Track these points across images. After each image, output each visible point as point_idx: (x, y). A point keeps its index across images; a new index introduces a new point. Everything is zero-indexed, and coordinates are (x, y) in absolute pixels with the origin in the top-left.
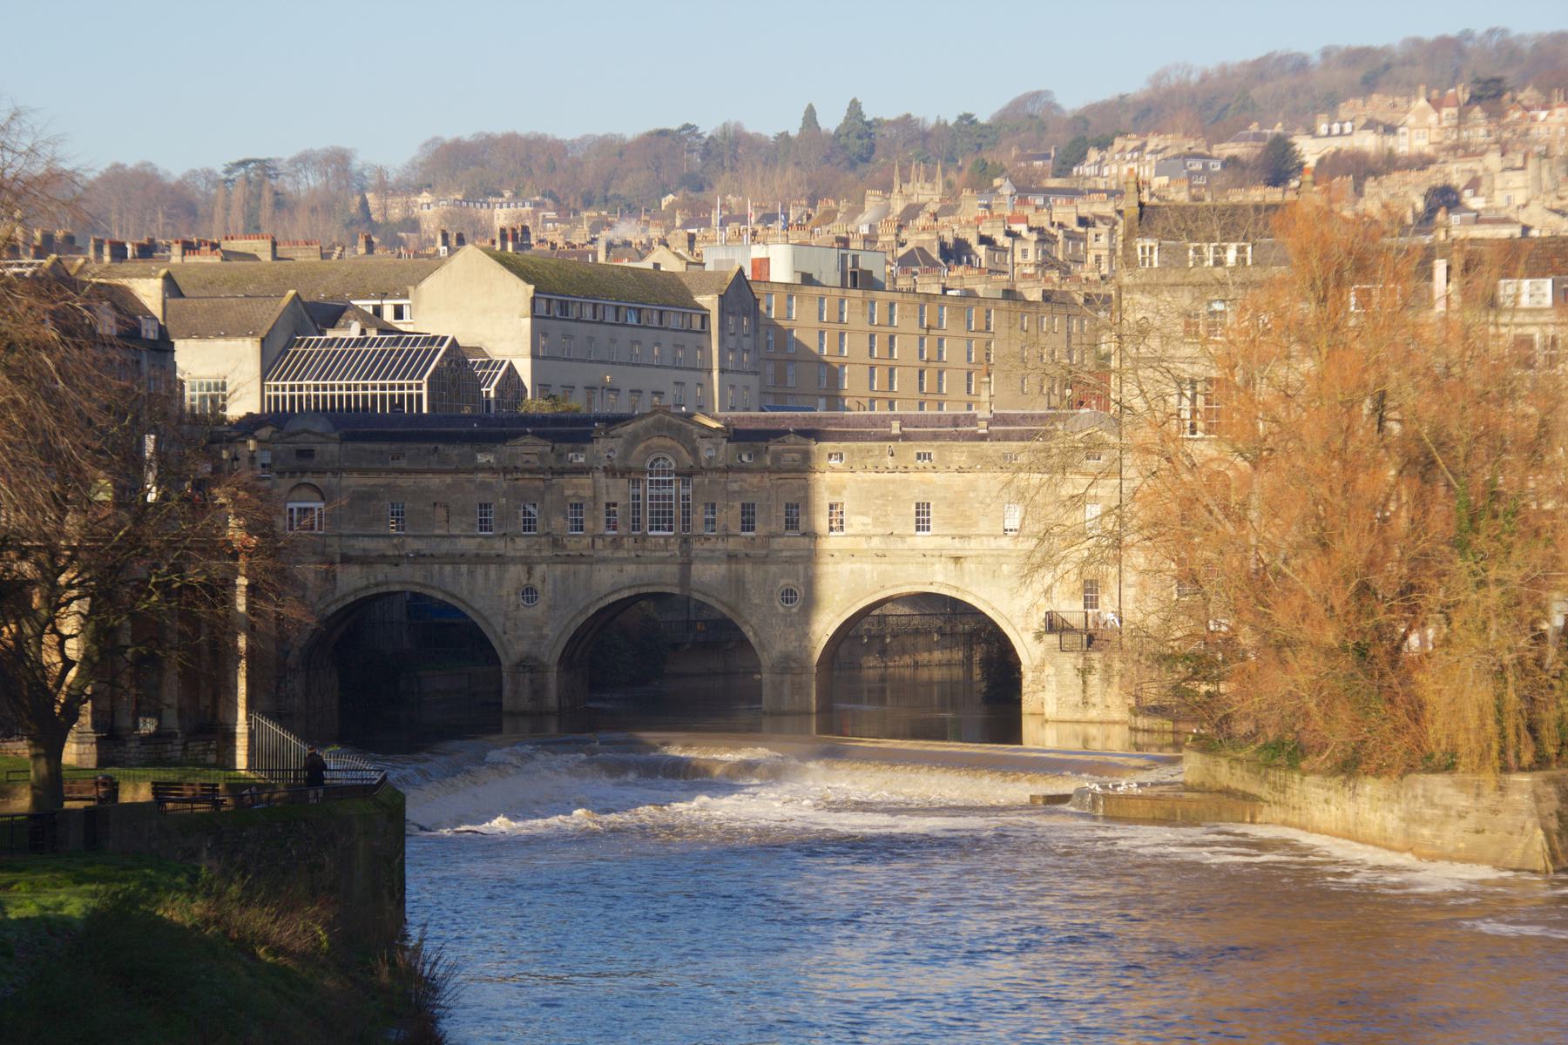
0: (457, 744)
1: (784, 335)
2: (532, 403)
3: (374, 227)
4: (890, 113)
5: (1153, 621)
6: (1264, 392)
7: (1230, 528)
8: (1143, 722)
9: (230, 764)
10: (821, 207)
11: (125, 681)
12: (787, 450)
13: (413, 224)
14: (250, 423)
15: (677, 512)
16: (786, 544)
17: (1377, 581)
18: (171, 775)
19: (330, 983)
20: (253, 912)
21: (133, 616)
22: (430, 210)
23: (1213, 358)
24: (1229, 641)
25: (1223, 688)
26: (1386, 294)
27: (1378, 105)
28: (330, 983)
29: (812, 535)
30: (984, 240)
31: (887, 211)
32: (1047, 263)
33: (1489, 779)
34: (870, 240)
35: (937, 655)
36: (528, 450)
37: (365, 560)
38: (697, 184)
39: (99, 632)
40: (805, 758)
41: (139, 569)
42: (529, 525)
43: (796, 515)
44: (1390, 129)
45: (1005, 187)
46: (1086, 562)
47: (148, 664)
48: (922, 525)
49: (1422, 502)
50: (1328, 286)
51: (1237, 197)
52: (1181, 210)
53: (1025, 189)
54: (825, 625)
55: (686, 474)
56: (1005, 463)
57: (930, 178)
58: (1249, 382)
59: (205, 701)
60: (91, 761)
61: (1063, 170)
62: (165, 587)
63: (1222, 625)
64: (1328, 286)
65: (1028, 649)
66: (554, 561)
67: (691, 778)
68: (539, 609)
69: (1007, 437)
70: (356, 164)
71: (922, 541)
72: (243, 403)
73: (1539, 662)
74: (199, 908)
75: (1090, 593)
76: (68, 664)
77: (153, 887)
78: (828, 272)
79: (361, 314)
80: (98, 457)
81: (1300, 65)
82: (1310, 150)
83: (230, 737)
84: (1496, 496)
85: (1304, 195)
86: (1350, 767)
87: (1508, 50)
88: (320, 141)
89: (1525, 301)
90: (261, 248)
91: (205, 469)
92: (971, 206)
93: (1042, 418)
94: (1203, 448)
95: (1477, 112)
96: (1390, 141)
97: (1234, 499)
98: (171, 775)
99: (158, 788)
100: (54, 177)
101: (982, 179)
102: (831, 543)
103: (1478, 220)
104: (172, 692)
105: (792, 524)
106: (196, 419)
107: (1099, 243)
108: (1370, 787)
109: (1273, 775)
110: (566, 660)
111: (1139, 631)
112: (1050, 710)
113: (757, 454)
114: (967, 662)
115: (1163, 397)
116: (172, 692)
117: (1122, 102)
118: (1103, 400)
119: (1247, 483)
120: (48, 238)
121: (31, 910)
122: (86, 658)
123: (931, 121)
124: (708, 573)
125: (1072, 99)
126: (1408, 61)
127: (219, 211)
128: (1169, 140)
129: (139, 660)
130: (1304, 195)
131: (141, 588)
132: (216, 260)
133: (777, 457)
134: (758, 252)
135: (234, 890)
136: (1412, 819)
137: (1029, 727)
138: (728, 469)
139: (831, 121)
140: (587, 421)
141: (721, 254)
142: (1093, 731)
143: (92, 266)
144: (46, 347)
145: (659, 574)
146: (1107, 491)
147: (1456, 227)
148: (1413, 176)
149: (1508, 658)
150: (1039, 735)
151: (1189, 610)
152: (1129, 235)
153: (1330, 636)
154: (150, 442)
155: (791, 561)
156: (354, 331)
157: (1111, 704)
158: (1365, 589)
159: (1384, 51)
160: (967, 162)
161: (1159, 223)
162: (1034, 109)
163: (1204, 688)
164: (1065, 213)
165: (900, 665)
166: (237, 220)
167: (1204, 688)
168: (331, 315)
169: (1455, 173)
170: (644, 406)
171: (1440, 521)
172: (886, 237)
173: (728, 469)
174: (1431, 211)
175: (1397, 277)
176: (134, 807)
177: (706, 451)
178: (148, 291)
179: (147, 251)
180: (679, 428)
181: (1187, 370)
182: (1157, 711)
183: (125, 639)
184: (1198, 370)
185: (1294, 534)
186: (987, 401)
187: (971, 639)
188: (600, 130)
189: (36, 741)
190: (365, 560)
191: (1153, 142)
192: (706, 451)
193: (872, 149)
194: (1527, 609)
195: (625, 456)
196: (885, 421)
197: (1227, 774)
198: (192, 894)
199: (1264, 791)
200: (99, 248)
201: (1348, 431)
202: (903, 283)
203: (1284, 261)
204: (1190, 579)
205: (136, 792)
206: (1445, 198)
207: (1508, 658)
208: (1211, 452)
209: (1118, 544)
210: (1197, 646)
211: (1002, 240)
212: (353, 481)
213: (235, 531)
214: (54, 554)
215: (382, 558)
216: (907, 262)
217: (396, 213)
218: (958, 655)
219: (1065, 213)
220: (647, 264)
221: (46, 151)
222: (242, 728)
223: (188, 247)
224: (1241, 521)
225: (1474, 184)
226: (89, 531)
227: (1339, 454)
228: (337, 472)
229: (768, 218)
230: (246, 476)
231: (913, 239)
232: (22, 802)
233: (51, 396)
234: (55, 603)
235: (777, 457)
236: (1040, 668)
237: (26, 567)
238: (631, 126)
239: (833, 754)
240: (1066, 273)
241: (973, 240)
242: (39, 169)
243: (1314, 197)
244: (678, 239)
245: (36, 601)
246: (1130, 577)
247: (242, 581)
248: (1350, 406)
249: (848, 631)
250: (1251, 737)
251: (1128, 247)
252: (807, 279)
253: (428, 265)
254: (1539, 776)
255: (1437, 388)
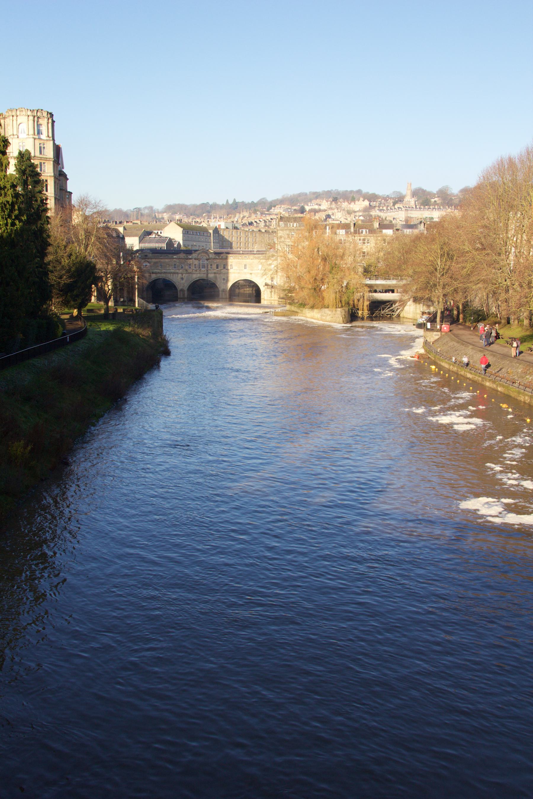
0: (171, 303)
1: (223, 237)
2: (182, 248)
3: (157, 219)
4: (240, 201)
5: (282, 284)
6: (300, 247)
7: (294, 269)
8: (280, 300)
9: (134, 305)
10: (230, 216)
11: (118, 292)
12: (224, 255)
13: (163, 218)
14: (137, 251)
15: (206, 266)
16: (224, 271)
17: (317, 278)
18: (126, 307)
19: (151, 341)
20: (139, 329)
21: (119, 282)
22: (166, 216)
23: (292, 242)
24: (294, 287)
25: (293, 295)
26: (319, 232)
27: (318, 201)
28: (151, 341)
29: (228, 270)
30: (255, 222)
31: (240, 217)
32: (266, 226)
33: (334, 309)
34: (237, 221)
35: (248, 289)
36: (182, 255)
37: (156, 273)
38: (209, 212)
39: (114, 285)
40: (226, 305)
41: (120, 274)
42: (182, 268)
43: (225, 266)
44: (320, 205)
45: (259, 213)
46: (272, 274)
47: (122, 290)
48: (245, 268)
49: (324, 265)
50: (310, 230)
51: (296, 215)
52: (287, 217)
53: (262, 214)
54: (230, 284)
55: (207, 260)
56: (258, 258)
57: (247, 211)
58: (298, 245)
59: (131, 296)
60: (113, 305)
61: (268, 210)
62: (124, 277)
63: (293, 285)
64: (310, 230)
65: (262, 288)
66: (186, 273)
67: (208, 308)
68: (184, 281)
69: (259, 254)
70: (154, 208)
71: (245, 271)
72: (136, 247)
73: (342, 291)
74: (131, 329)
75: (272, 279)
76: (109, 290)
77: (123, 325)
78: (230, 227)
79: (155, 233)
80: (113, 256)
81: (306, 194)
82: (307, 208)
83: (135, 302)
84: (336, 264)
85: (306, 215)
86: (313, 307)
87: (338, 193)
88: (148, 205)
89: (341, 234)
90: (139, 222)
91: (130, 258)
92: (253, 216)
93: (265, 251)
94: (290, 256)
95: (333, 203)
96: (320, 207)
97: (295, 264)
98: (126, 307)
99: (124, 310)
100: (106, 211)
101: (255, 212)
102: (231, 271)
103: (333, 220)
104: (125, 294)
105: (224, 268)
106: (129, 250)
107: (274, 223)
108: (316, 311)
109: (301, 309)
110: (188, 289)
111: (280, 286)
112: (266, 298)
113: (219, 256)
114: (253, 290)
115: (284, 248)
116: (125, 294)
117: (277, 200)
118: (275, 248)
119: (297, 262)
120: (105, 220)
121: (104, 329)
122: (112, 289)
123: (247, 202)
124: (211, 276)
125: (270, 199)
126: (323, 194)
127: (132, 216)
128: (285, 206)
129: (120, 289)
130: (306, 215)
131: (120, 277)
132: (132, 224)
133: (222, 257)
134: (219, 223)
135: (136, 326)
136: (322, 316)
137: (262, 301)
138: (214, 259)
139: (231, 202)
140: (191, 251)
141: (213, 224)
142: (272, 301)
143: (112, 225)
144: (105, 238)
145: (203, 276)
146: (275, 263)
147: (330, 221)
148: (323, 213)
149: (337, 290)
150: (264, 302)
151: (288, 282)
152: (279, 221)
153: (310, 287)
154: (121, 254)
155: (224, 274)
156: (154, 236)
157: (275, 297)
158: (315, 279)
159: (319, 192)
160: (253, 209)
161: (284, 220)
162: (263, 200)
163: (290, 295)
164: (269, 218)
165: (242, 291)
166: (135, 217)
167: (290, 295)
168: (150, 233)
169: (330, 212)
170: (201, 248)
171: (327, 268)
172: (240, 221)
173: (214, 259)
174: (326, 218)
175: (321, 229)
176: (120, 313)
177: (211, 256)
178: (121, 229)
179: (120, 223)
180: (206, 252)
181: (288, 244)
182: (283, 298)
183: (118, 286)
184: (290, 243)
185: (304, 270)
186: (256, 248)
187: (253, 287)
188: (193, 203)
189: (105, 302)
190: (156, 273)
191: (282, 206)
192: (211, 256)
193: (237, 207)
194: (340, 282)
195: (198, 256)
196: (239, 251)
197: (293, 308)
198: (129, 326)
199: (299, 311)
200: (113, 222)
201: (313, 254)
202: (242, 229)
203: (304, 226)
204: (288, 277)
205: (120, 310)
206: (328, 216)
207: (337, 290)
208: (292, 257)
209: (277, 271)
210: (288, 288)
211: (258, 222)
212: (154, 260)
213: (135, 268)
214: (107, 272)
215: (159, 273)
216: (243, 225)
217: (160, 217)
218: (251, 289)
219: (269, 218)
220: (201, 225)
221: (105, 207)
222: (137, 300)
223: (127, 222)
224: (296, 268)
225: (333, 214)
226: (112, 268)
227: (312, 257)
228: (151, 259)
229: (221, 218)
230: (137, 259)
231: (244, 222)
232: (103, 312)
233: (106, 246)
234: (107, 280)
235: (222, 257)
236: (264, 291)
237: (102, 274)
238: (198, 203)
239: (231, 305)
240: (269, 227)
241: (254, 222)
242: (103, 209)
243: (308, 216)
244: (206, 221)
245: (104, 280)
246: (279, 277)
247: (136, 277)
248: (314, 250)
249: (234, 285)
250: (297, 303)
251: (279, 223)
252: (227, 228)
253: (165, 225)
254: (342, 309)
255: (327, 247)
